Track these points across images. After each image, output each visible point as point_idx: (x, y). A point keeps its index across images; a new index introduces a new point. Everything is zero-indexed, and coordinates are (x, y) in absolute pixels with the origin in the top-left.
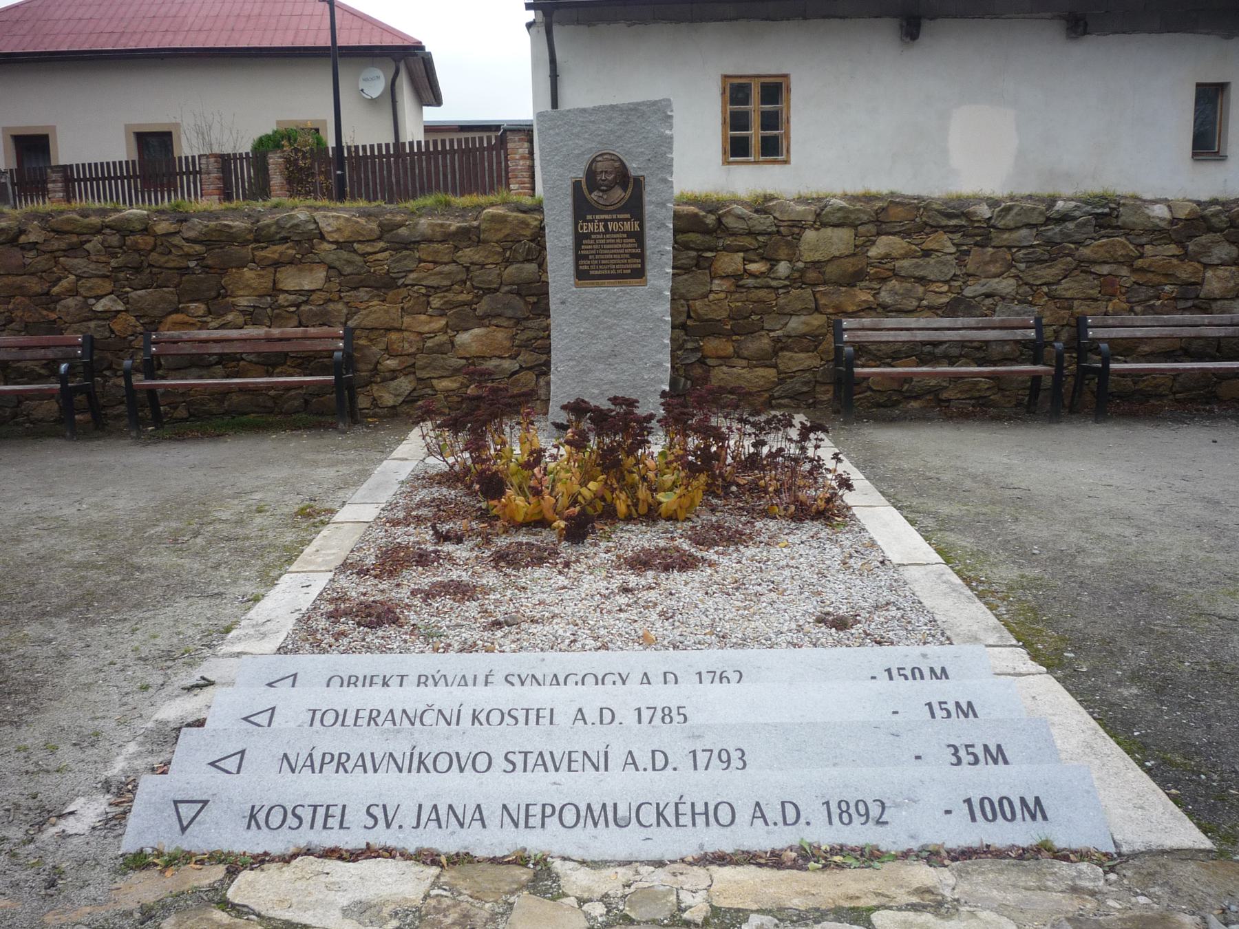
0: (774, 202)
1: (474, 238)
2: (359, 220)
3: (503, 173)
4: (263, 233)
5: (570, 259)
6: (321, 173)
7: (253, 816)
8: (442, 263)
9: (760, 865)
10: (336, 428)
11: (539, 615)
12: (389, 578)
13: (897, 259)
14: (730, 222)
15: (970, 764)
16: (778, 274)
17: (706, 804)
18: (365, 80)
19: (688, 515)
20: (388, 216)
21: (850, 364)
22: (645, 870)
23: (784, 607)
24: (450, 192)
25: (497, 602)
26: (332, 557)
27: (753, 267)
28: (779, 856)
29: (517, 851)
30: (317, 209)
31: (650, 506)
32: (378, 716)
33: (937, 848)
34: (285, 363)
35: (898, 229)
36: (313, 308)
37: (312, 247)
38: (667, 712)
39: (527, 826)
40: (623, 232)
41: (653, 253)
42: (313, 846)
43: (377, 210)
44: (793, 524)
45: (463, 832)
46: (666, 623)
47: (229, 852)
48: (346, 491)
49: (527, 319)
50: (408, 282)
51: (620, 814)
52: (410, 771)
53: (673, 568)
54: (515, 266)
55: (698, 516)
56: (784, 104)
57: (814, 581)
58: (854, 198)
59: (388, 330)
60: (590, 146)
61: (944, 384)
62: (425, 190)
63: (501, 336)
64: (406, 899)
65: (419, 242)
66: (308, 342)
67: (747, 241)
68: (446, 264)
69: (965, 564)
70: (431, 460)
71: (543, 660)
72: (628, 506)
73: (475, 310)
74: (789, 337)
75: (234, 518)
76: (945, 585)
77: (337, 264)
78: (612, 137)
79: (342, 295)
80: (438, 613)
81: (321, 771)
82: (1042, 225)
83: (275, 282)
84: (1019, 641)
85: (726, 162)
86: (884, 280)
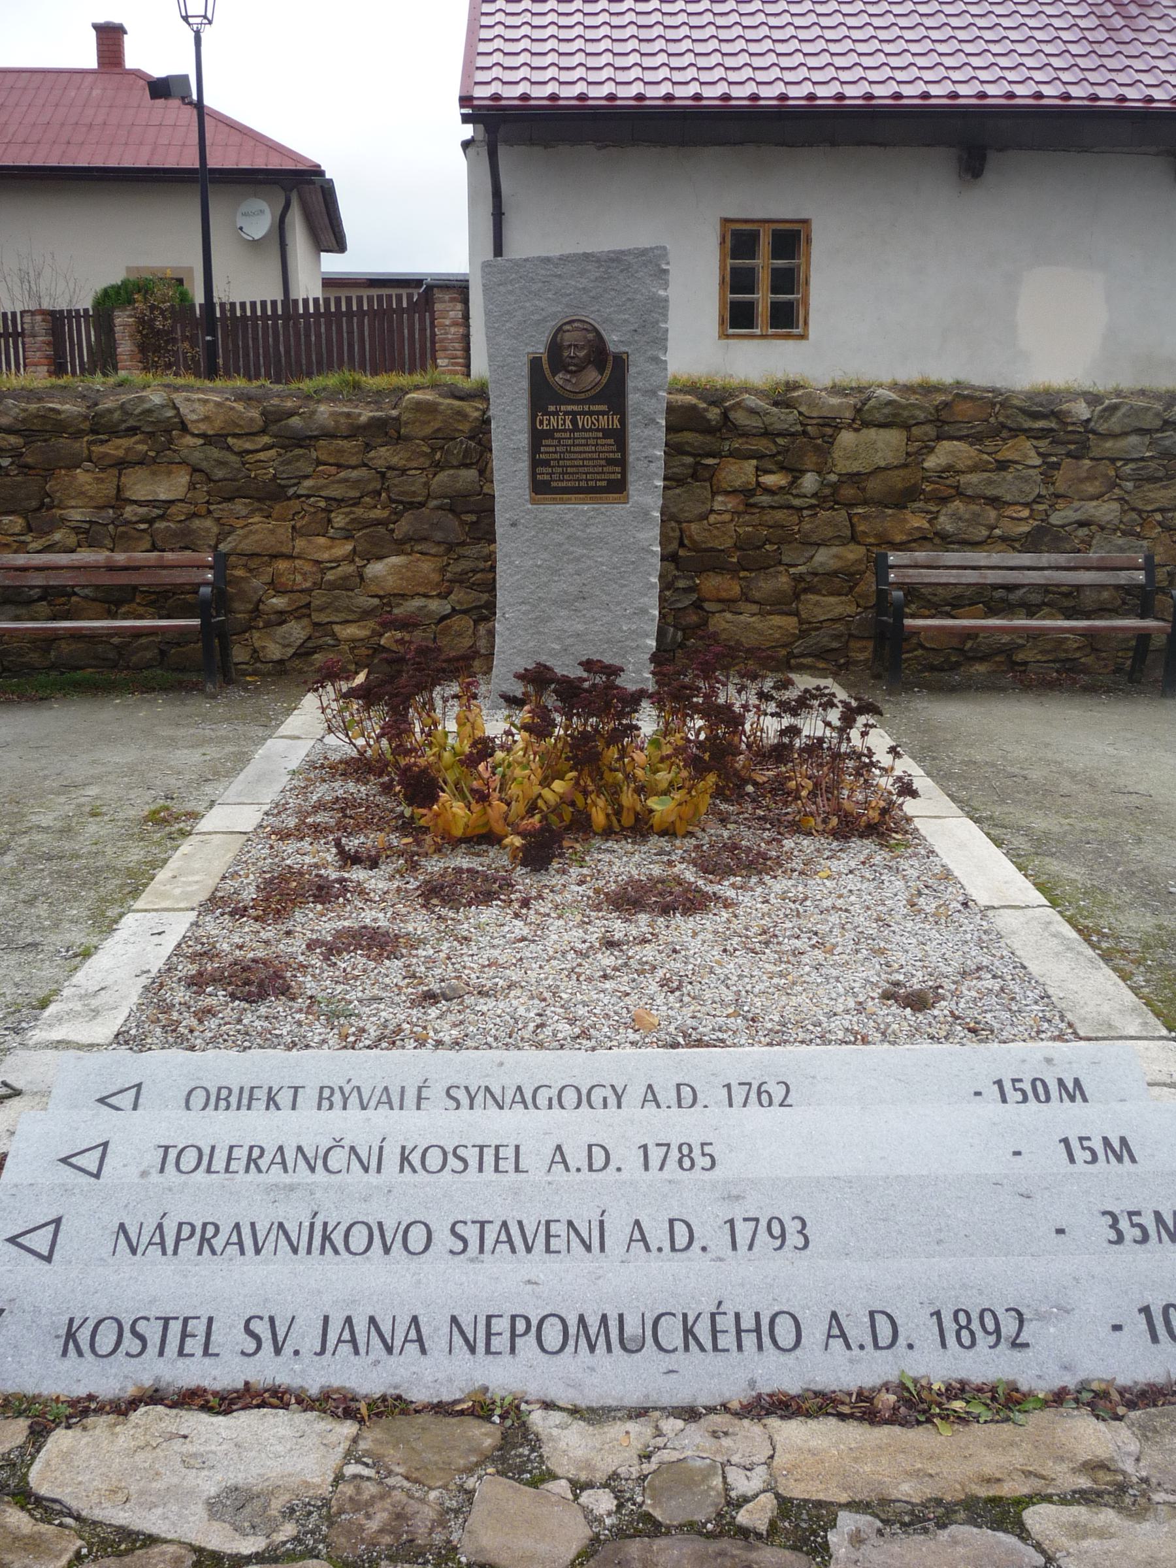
0: (800, 392)
1: (392, 432)
2: (234, 405)
3: (428, 344)
4: (102, 421)
5: (524, 465)
6: (185, 338)
7: (71, 1336)
8: (349, 467)
9: (842, 1417)
10: (202, 691)
11: (489, 984)
12: (275, 921)
13: (963, 472)
14: (739, 417)
15: (1135, 1241)
16: (803, 490)
17: (757, 1315)
18: (245, 214)
19: (690, 828)
20: (275, 401)
21: (900, 615)
22: (671, 1425)
23: (835, 973)
24: (368, 373)
25: (430, 962)
26: (195, 887)
27: (770, 480)
28: (870, 1400)
29: (475, 1392)
30: (177, 389)
31: (637, 814)
32: (261, 1156)
33: (1103, 1386)
34: (132, 600)
35: (965, 432)
36: (172, 525)
37: (171, 442)
38: (685, 1151)
39: (488, 1351)
40: (598, 430)
41: (638, 459)
42: (163, 1384)
43: (260, 391)
44: (835, 843)
45: (393, 1360)
46: (671, 998)
47: (34, 1397)
48: (215, 784)
49: (463, 544)
50: (300, 492)
51: (629, 1331)
52: (309, 1252)
53: (675, 909)
54: (447, 472)
55: (703, 830)
56: (803, 260)
57: (874, 932)
58: (908, 389)
59: (274, 557)
60: (554, 309)
61: (1020, 641)
62: (324, 366)
63: (427, 567)
64: (307, 1485)
65: (316, 438)
66: (165, 572)
67: (762, 445)
68: (354, 468)
69: (1078, 907)
70: (331, 740)
71: (501, 1064)
72: (608, 815)
73: (393, 531)
74: (816, 574)
75: (59, 824)
76: (1056, 941)
77: (204, 465)
78: (585, 298)
79: (212, 507)
80: (346, 978)
81: (175, 1252)
82: (1157, 431)
83: (119, 489)
84: (1170, 1030)
85: (724, 336)
86: (944, 500)
